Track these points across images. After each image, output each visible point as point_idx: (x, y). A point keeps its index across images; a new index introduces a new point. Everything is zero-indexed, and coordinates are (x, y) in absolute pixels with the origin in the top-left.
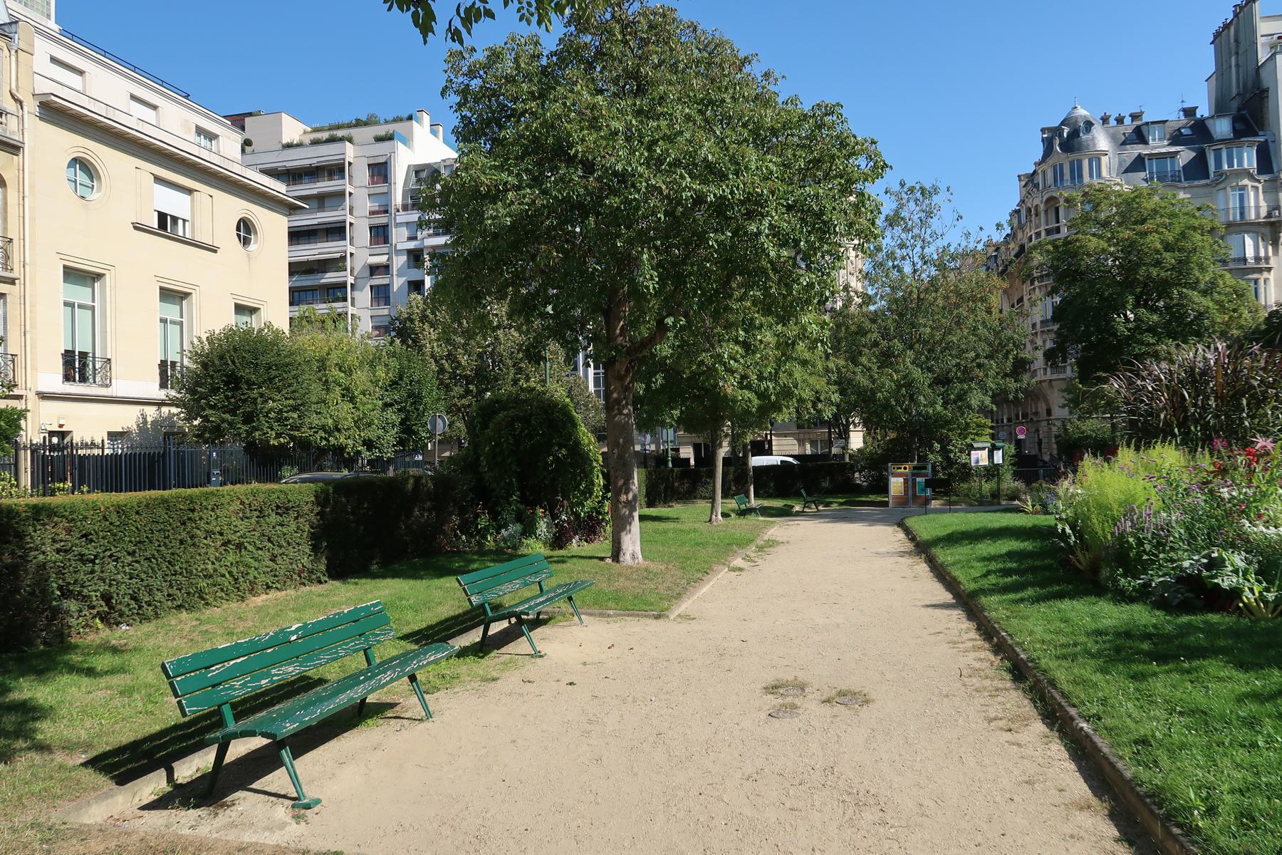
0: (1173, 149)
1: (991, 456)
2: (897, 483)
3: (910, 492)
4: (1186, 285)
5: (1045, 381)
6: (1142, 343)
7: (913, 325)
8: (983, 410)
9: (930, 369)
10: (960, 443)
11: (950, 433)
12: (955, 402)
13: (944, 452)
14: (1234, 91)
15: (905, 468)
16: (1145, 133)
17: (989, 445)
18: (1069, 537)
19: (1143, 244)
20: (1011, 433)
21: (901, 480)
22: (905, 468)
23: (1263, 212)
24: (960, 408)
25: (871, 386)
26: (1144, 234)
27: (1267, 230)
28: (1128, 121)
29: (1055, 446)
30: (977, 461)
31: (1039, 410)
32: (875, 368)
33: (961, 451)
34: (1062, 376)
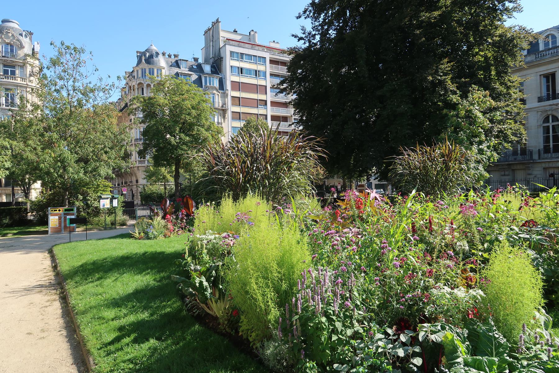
0: (190, 73)
1: (111, 202)
2: (54, 219)
3: (63, 225)
4: (199, 126)
5: (136, 167)
6: (182, 149)
7: (66, 125)
8: (107, 178)
9: (76, 153)
10: (94, 196)
11: (88, 190)
12: (91, 172)
13: (85, 200)
14: (211, 56)
15: (59, 210)
16: (180, 64)
17: (110, 196)
18: (206, 290)
19: (183, 105)
20: (119, 191)
21: (57, 217)
22: (59, 210)
23: (221, 105)
24: (94, 175)
25: (37, 159)
26: (183, 100)
27: (221, 112)
28: (173, 57)
29: (140, 197)
30: (104, 206)
31: (133, 180)
32: (39, 148)
33: (95, 200)
34: (143, 165)
